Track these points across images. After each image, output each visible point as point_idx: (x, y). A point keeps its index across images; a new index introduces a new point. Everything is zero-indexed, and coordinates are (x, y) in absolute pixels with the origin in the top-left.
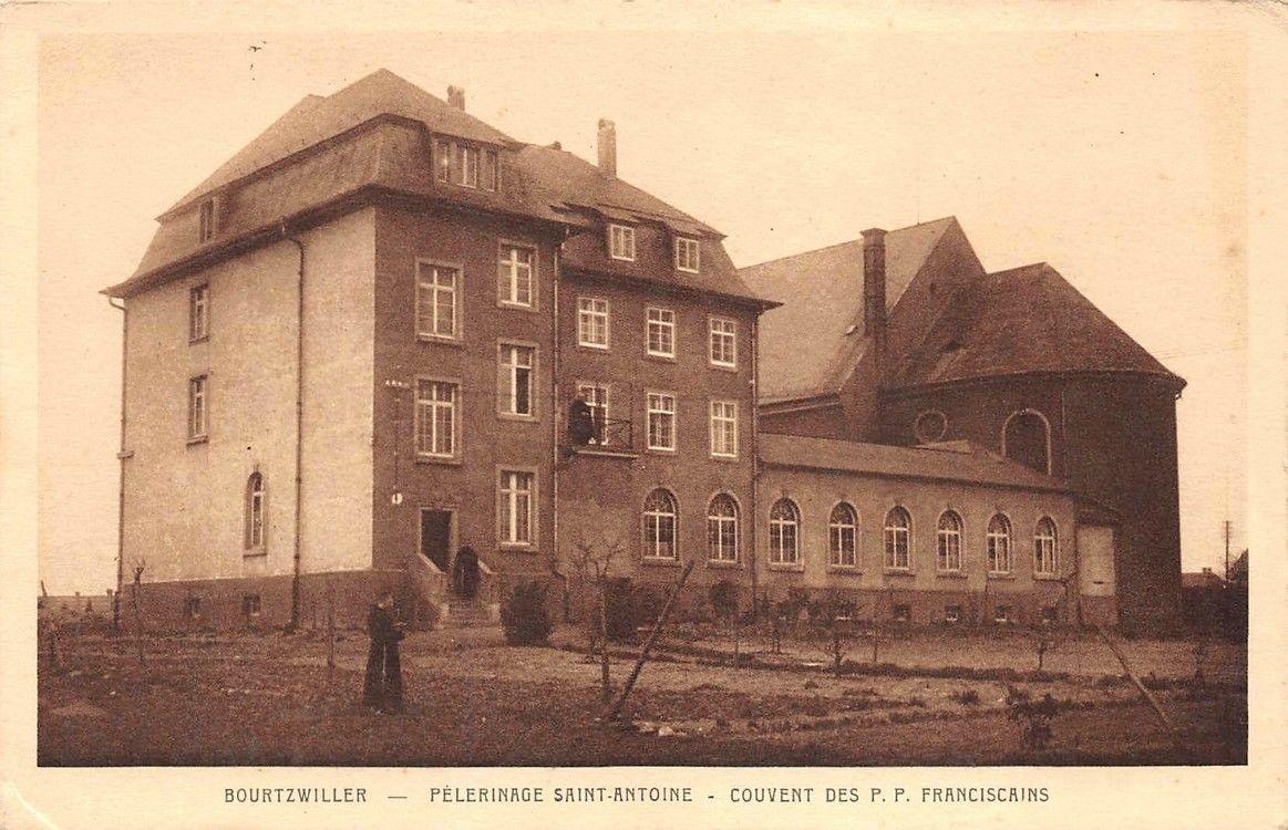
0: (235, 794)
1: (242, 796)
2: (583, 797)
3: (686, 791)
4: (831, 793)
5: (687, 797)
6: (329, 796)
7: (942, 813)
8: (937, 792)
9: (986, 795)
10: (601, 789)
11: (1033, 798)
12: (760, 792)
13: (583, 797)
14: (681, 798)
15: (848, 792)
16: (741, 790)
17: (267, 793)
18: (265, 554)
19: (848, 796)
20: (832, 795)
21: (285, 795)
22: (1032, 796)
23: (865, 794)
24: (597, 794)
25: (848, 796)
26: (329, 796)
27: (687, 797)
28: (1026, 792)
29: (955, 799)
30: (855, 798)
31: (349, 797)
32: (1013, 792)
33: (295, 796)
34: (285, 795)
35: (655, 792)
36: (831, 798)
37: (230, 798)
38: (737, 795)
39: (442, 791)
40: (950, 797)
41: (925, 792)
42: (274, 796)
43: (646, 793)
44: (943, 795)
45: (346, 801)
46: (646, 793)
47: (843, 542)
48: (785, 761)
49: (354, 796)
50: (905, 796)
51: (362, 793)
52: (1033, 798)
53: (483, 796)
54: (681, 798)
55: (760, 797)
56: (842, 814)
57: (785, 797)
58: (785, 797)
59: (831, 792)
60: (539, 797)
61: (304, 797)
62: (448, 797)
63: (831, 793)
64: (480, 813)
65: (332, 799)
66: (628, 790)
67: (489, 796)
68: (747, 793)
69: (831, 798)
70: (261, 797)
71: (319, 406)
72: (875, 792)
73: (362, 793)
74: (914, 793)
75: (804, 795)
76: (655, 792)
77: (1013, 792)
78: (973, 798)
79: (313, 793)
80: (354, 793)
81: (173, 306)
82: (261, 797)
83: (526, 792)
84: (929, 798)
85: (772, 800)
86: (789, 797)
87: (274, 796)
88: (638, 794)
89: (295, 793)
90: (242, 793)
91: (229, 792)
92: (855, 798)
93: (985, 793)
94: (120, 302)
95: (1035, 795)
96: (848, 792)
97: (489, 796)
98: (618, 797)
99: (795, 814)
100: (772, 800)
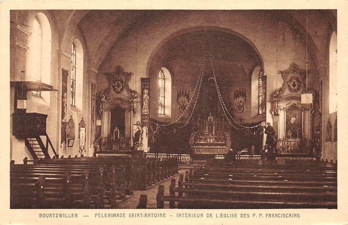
0: (42, 215)
1: (44, 216)
2: (294, 216)
5: (211, 216)
7: (224, 220)
8: (270, 215)
9: (283, 216)
12: (47, 215)
13: (294, 216)
14: (163, 216)
16: (154, 214)
17: (51, 215)
18: (72, 146)
21: (55, 215)
22: (295, 216)
23: (251, 215)
24: (140, 215)
25: (247, 216)
28: (136, 215)
29: (275, 217)
33: (58, 215)
34: (55, 215)
37: (41, 216)
42: (53, 216)
43: (153, 215)
44: (271, 216)
46: (153, 215)
48: (54, 207)
49: (74, 216)
51: (76, 215)
53: (76, 216)
54: (163, 216)
55: (47, 216)
57: (186, 216)
61: (61, 216)
63: (242, 215)
66: (148, 214)
68: (44, 216)
69: (208, 216)
71: (340, 47)
72: (254, 215)
73: (76, 215)
74: (264, 215)
79: (63, 215)
80: (108, 215)
84: (268, 216)
86: (188, 216)
88: (151, 215)
89: (58, 215)
91: (96, 214)
93: (231, 215)
95: (296, 216)
97: (111, 216)
99: (201, 220)
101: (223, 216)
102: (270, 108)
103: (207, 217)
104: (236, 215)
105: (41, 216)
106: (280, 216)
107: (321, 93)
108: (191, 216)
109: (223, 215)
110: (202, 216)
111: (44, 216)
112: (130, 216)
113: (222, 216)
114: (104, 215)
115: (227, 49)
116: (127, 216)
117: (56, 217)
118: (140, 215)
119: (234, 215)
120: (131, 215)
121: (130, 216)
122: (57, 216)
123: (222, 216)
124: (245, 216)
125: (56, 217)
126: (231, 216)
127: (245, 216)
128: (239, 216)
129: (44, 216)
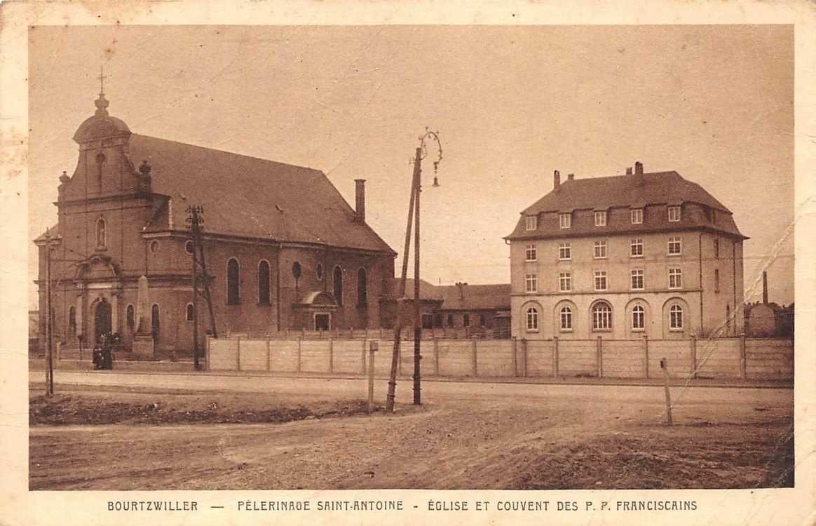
0: (114, 505)
1: (507, 507)
2: (683, 507)
3: (306, 503)
4: (560, 504)
5: (400, 507)
6: (174, 506)
8: (626, 504)
9: (658, 506)
10: (371, 502)
11: (687, 507)
12: (515, 504)
13: (683, 507)
15: (571, 504)
17: (134, 504)
19: (571, 507)
20: (562, 506)
23: (582, 505)
24: (344, 506)
25: (571, 507)
26: (174, 506)
27: (400, 507)
28: (388, 504)
29: (360, 509)
30: (575, 508)
31: (264, 507)
32: (675, 504)
33: (152, 506)
34: (146, 506)
35: (379, 504)
36: (560, 508)
38: (501, 506)
39: (245, 503)
40: (634, 507)
41: (618, 504)
43: (374, 505)
44: (630, 506)
45: (255, 509)
46: (374, 505)
47: (357, 357)
50: (592, 507)
52: (687, 507)
53: (134, 507)
55: (515, 508)
56: (567, 517)
57: (531, 508)
58: (531, 508)
59: (560, 504)
60: (307, 507)
61: (158, 507)
62: (249, 507)
64: (271, 516)
65: (450, 509)
67: (275, 506)
69: (560, 508)
70: (130, 508)
72: (589, 504)
73: (194, 505)
75: (543, 506)
76: (379, 504)
77: (675, 504)
78: (650, 508)
79: (163, 504)
81: (523, 249)
82: (130, 508)
83: (118, 504)
84: (621, 508)
85: (523, 509)
86: (534, 507)
87: (139, 506)
88: (369, 505)
90: (118, 507)
91: (110, 504)
92: (575, 508)
94: (509, 242)
96: (571, 504)
97: (275, 506)
98: (356, 507)
100: (523, 509)
101: (434, 507)
102: (75, 151)
103: (109, 510)
104: (464, 504)
105: (111, 508)
106: (651, 506)
107: (709, 384)
108: (276, 508)
109: (435, 504)
110: (134, 507)
111: (507, 507)
112: (321, 508)
113: (431, 507)
114: (259, 506)
115: (729, 140)
116: (553, 506)
117: (148, 509)
118: (543, 506)
119: (461, 505)
120: (323, 504)
121: (321, 508)
122: (150, 508)
123: (431, 507)
124: (568, 508)
125: (148, 509)
126: (454, 507)
127: (568, 508)
128: (313, 506)
129: (118, 507)
